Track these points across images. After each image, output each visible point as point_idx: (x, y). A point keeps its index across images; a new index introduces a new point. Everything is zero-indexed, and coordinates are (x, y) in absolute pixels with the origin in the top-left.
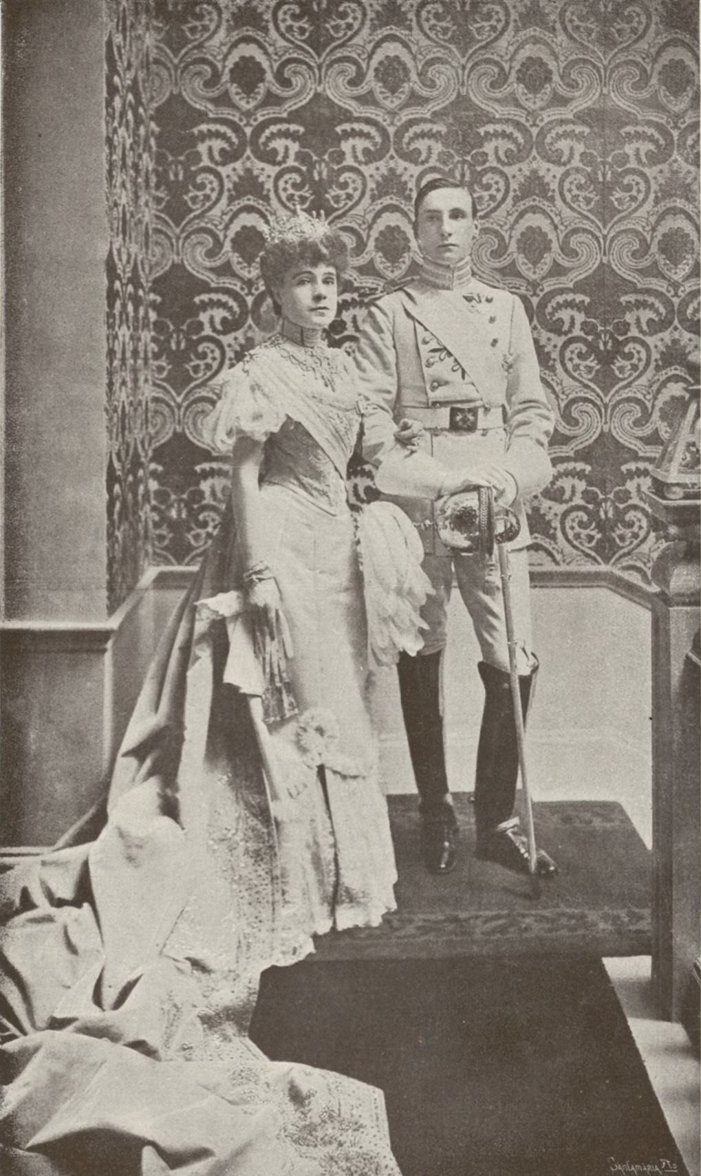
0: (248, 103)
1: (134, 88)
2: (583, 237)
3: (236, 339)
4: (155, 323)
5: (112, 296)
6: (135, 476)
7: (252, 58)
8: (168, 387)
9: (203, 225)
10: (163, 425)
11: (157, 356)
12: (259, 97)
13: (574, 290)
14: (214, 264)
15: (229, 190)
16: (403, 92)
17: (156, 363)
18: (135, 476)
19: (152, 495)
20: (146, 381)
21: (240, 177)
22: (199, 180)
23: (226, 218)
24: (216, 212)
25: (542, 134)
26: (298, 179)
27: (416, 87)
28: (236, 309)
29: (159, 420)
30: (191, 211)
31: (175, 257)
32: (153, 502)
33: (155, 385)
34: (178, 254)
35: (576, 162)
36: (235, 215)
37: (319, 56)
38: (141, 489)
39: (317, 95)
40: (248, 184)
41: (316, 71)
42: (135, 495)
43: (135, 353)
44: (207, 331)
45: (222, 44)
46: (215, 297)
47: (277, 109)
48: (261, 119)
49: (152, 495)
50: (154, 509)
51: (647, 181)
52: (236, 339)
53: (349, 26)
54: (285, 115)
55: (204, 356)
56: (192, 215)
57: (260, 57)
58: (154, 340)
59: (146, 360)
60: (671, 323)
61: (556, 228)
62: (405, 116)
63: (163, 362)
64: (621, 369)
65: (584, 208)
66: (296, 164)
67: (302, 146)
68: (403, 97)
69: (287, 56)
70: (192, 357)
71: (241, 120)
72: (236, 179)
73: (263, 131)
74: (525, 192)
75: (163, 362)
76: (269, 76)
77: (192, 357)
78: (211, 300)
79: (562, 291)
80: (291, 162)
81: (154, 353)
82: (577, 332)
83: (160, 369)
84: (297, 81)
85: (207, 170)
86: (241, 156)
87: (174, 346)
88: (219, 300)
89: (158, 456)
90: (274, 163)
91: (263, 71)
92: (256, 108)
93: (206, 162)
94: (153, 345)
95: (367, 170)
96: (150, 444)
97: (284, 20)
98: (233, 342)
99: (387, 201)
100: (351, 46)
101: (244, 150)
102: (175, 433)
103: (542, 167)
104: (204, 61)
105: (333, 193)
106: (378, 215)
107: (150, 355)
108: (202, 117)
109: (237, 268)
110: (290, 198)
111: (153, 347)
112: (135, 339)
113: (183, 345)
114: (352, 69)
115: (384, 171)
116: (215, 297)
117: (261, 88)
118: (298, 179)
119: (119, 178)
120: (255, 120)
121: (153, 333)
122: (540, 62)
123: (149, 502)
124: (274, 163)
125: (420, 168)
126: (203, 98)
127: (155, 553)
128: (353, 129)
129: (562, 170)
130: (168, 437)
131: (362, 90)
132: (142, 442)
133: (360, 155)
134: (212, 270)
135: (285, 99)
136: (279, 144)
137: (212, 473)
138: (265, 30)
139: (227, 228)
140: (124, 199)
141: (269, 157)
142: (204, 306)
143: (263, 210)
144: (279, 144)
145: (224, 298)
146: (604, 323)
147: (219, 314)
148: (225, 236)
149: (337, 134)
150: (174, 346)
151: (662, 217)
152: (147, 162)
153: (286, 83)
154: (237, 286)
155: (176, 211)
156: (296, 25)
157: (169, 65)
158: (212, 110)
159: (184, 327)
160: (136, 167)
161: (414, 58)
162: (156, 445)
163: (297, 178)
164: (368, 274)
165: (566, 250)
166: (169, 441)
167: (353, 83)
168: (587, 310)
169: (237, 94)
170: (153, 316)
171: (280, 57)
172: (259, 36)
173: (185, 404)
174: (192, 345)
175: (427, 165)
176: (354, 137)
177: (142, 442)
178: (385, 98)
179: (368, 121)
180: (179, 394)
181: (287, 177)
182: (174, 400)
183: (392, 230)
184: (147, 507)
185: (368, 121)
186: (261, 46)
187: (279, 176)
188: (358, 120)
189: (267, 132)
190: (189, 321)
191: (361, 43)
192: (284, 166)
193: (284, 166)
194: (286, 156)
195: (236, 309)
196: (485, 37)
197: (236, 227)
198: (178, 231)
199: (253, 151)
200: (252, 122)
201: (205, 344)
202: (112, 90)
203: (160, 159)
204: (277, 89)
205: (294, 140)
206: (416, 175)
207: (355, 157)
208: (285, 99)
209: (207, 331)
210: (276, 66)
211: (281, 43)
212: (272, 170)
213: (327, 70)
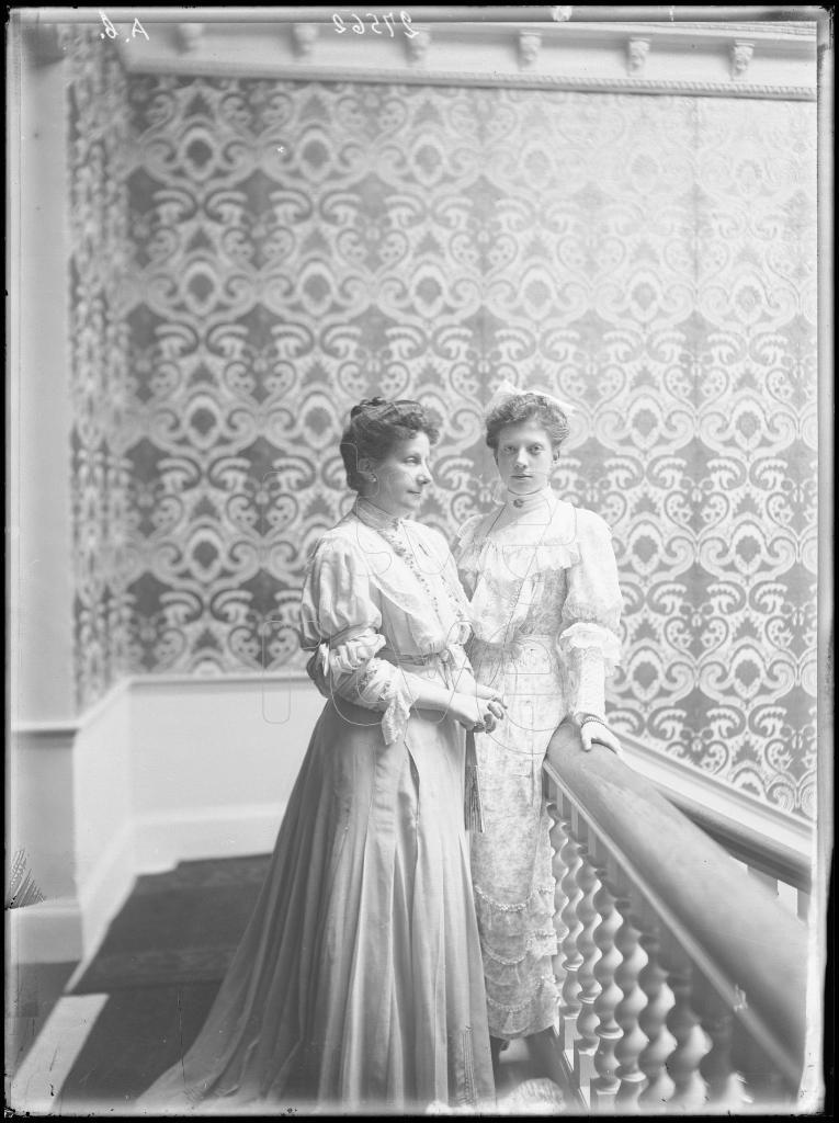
0: (646, 695)
1: (102, 296)
2: (678, 416)
3: (635, 493)
5: (76, 464)
13: (675, 456)
25: (437, 334)
30: (706, 398)
35: (570, 360)
43: (105, 508)
51: (624, 374)
60: (744, 481)
61: (661, 410)
62: (327, 321)
64: (708, 516)
65: (784, 398)
74: (423, 380)
79: (451, 457)
82: (464, 488)
85: (398, 363)
93: (613, 360)
97: (672, 633)
103: (437, 361)
104: (394, 279)
106: (307, 398)
110: (569, 387)
112: (104, 495)
114: (398, 286)
119: (84, 369)
122: (541, 283)
129: (558, 365)
133: (621, 356)
140: (91, 386)
141: (218, 351)
146: (697, 481)
148: (628, 544)
151: (192, 398)
152: (117, 356)
154: (193, 454)
158: (172, 315)
160: (105, 360)
163: (355, 369)
165: (771, 427)
168: (579, 471)
179: (729, 707)
183: (747, 415)
185: (729, 707)
194: (566, 356)
196: (389, 262)
198: (592, 412)
202: (76, 299)
203: (130, 353)
206: (765, 373)
207: (617, 356)
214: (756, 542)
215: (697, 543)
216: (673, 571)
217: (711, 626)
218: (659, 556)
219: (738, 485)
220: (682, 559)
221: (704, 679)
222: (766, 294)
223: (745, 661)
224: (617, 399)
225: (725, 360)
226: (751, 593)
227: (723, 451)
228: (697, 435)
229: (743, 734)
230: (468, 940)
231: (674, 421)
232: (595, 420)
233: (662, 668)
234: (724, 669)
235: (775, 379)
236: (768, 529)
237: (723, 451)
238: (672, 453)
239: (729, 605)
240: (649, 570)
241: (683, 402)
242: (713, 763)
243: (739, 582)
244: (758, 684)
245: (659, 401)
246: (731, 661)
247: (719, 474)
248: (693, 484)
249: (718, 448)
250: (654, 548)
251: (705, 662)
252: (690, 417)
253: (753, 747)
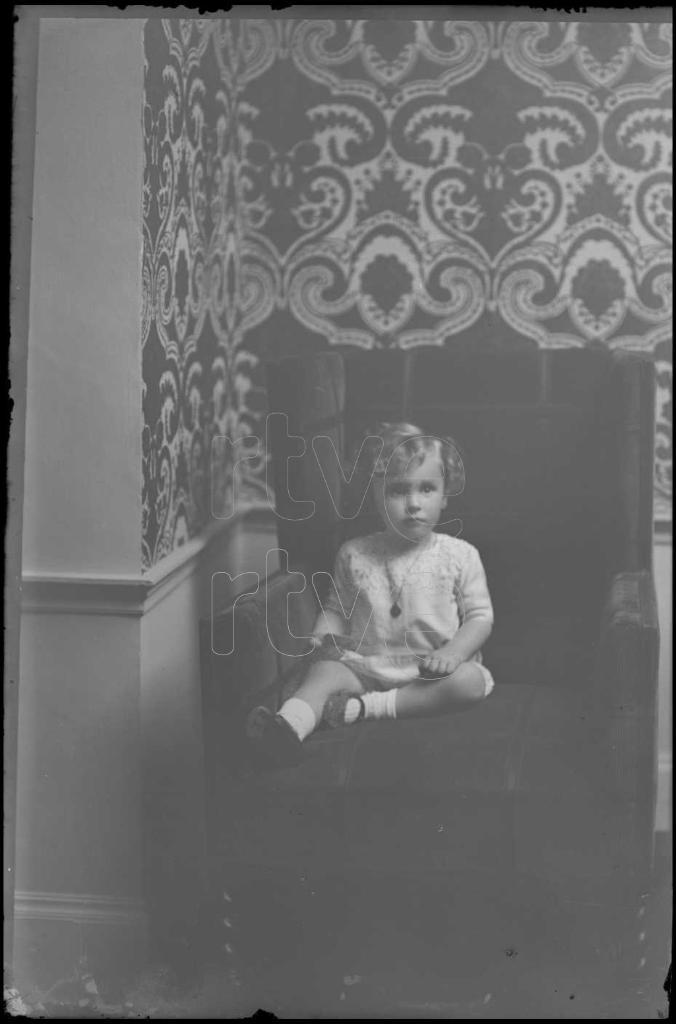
0: (389, 73)
4: (250, 147)
6: (207, 365)
7: (393, 259)
8: (267, 242)
9: (319, 253)
10: (260, 297)
11: (250, 196)
12: (406, 65)
13: (448, 101)
14: (336, 61)
15: (359, 202)
16: (614, 315)
17: (250, 206)
18: (207, 365)
19: (241, 399)
20: (231, 229)
21: (375, 182)
22: (315, 186)
23: (354, 244)
24: (339, 234)
26: (462, 188)
27: (635, 308)
28: (369, 128)
29: (253, 289)
31: (279, 300)
32: (243, 409)
33: (247, 238)
34: (282, 295)
36: (367, 240)
37: (492, 256)
38: (220, 388)
39: (491, 63)
40: (388, 195)
41: (487, 278)
42: (207, 394)
44: (325, 160)
45: (350, 237)
46: (337, 109)
47: (431, 84)
48: (407, 98)
49: (241, 399)
50: (243, 418)
52: (367, 172)
53: (536, 216)
54: (443, 92)
55: (318, 197)
56: (303, 239)
57: (405, 257)
58: (245, 171)
59: (231, 197)
63: (259, 205)
66: (458, 165)
67: (468, 138)
68: (620, 68)
69: (444, 256)
70: (303, 198)
71: (379, 99)
72: (370, 187)
73: (410, 115)
75: (259, 205)
76: (418, 285)
77: (303, 198)
78: (332, 114)
80: (451, 162)
81: (245, 190)
83: (256, 216)
84: (459, 293)
86: (378, 153)
87: (275, 182)
88: (343, 116)
89: (250, 342)
90: (425, 163)
91: (409, 278)
92: (404, 81)
94: (245, 180)
95: (563, 177)
96: (237, 323)
97: (442, 203)
98: (362, 177)
99: (591, 224)
100: (540, 244)
101: (382, 145)
102: (277, 61)
105: (512, 211)
107: (239, 193)
108: (324, 95)
109: (369, 316)
111: (246, 182)
113: (289, 181)
115: (588, 178)
116: (337, 109)
117: (407, 302)
118: (462, 188)
120: (400, 99)
121: (245, 162)
123: (235, 406)
124: (426, 164)
125: (642, 176)
126: (320, 316)
127: (245, 482)
128: (543, 116)
130: (265, 315)
131: (554, 310)
132: (223, 320)
134: (333, 68)
135: (440, 319)
136: (434, 136)
137: (333, 120)
138: (414, 217)
139: (354, 258)
141: (419, 154)
142: (323, 123)
143: (408, 231)
144: (434, 136)
145: (351, 112)
147: (343, 135)
148: (352, 271)
149: (516, 120)
150: (275, 182)
153: (440, 294)
155: (282, 231)
156: (459, 210)
157: (273, 266)
159: (291, 154)
161: (632, 263)
162: (248, 324)
164: (560, 330)
166: (266, 323)
167: (542, 299)
169: (374, 60)
170: (245, 136)
171: (435, 256)
172: (404, 224)
173: (292, 267)
174: (303, 181)
175: (652, 172)
176: (544, 127)
177: (223, 320)
178: (592, 70)
179: (564, 104)
180: (282, 252)
181: (444, 184)
182: (276, 261)
184: (233, 416)
185: (564, 104)
186: (407, 240)
187: (433, 182)
188: (550, 102)
189: (417, 118)
190: (300, 143)
191: (553, 240)
192: (440, 168)
193: (440, 168)
195: (369, 128)
197: (368, 256)
199: (395, 145)
200: (395, 101)
201: (322, 180)
204: (430, 306)
205: (456, 131)
208: (440, 319)
209: (325, 160)
210: (428, 269)
211: (436, 236)
212: (423, 174)
213: (502, 280)
214: (616, 272)
215: (492, 273)
216: (442, 328)
217: (525, 190)
218: (414, 296)
219: (580, 160)
220: (459, 304)
221: (507, 292)
222: (634, 277)
223: (592, 262)
224: (333, 235)
225: (553, 157)
226: (608, 123)
227: (551, 88)
228: (492, 306)
229: (593, 159)
230: (31, 196)
231: (445, 279)
232: (287, 277)
233: (421, 271)
234: (548, 276)
235: (655, 196)
236: (640, 249)
237: (551, 88)
238: (443, 92)
239: (561, 148)
240: (397, 75)
241: (465, 244)
242: (527, 216)
243: (583, 101)
244: (625, 58)
245: (415, 239)
246: (566, 262)
247: (540, 135)
248: (486, 156)
249: (541, 80)
250: (404, 281)
251: (511, 262)
252: (477, 272)
253: (612, 187)
